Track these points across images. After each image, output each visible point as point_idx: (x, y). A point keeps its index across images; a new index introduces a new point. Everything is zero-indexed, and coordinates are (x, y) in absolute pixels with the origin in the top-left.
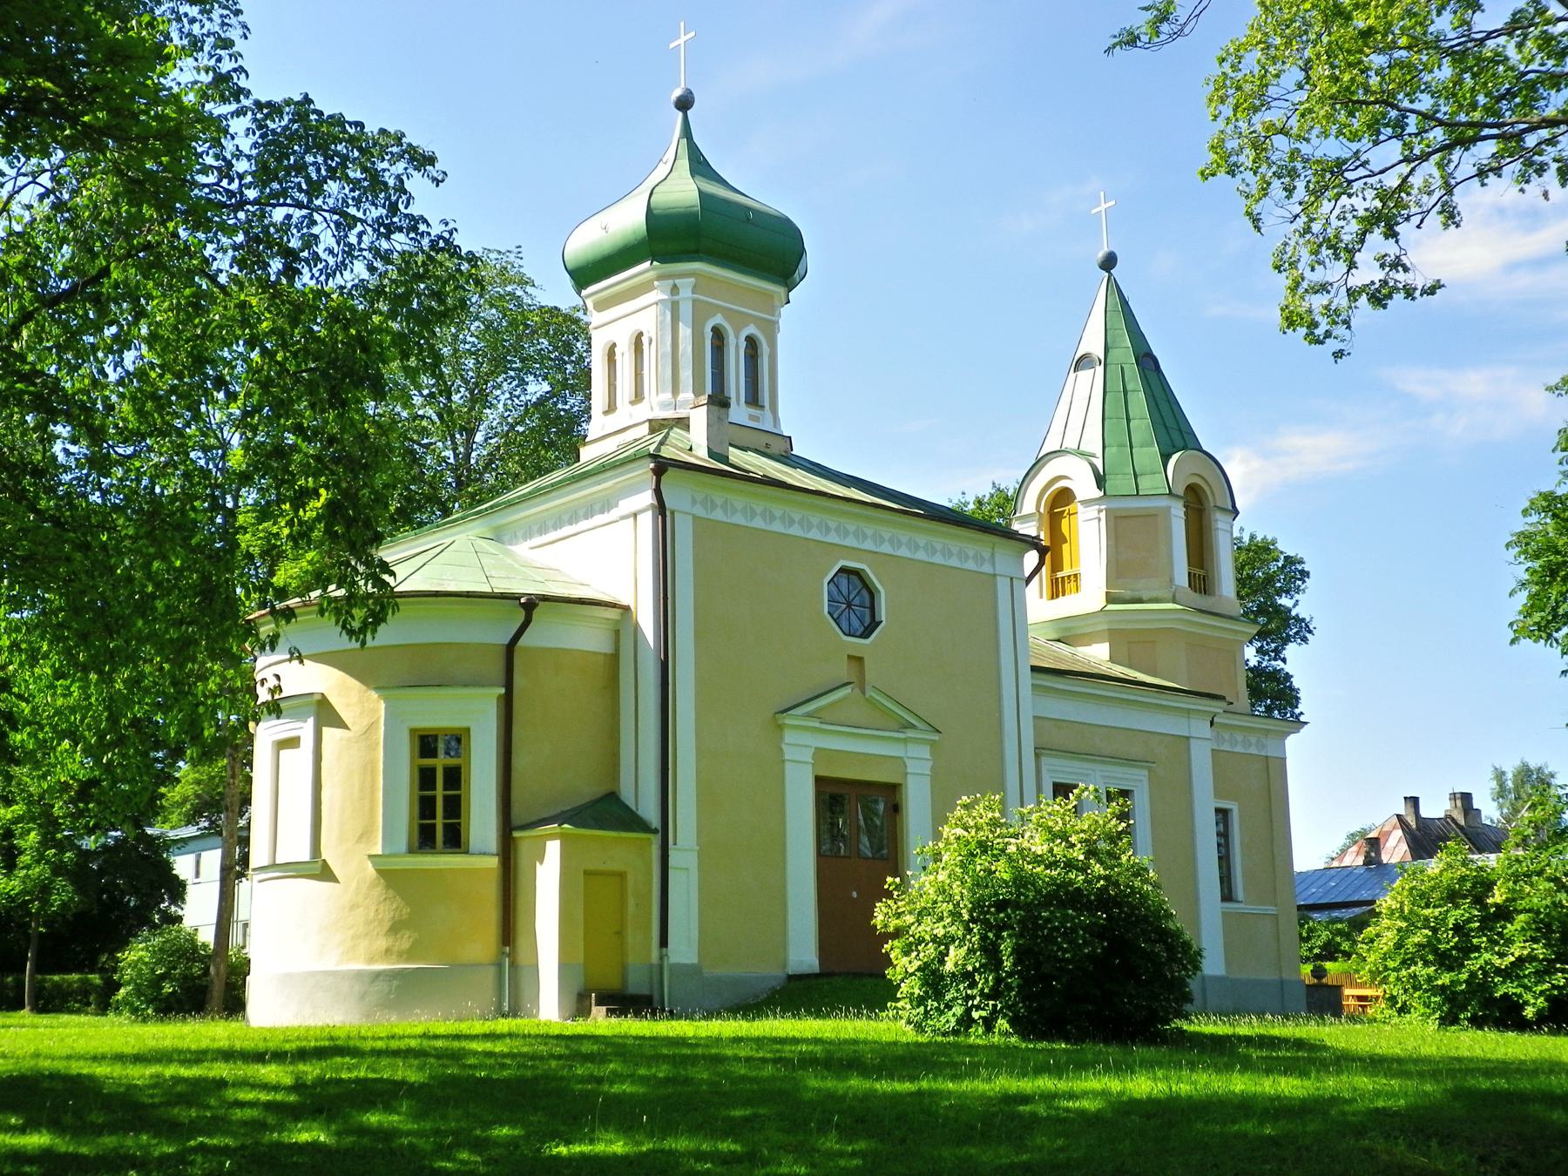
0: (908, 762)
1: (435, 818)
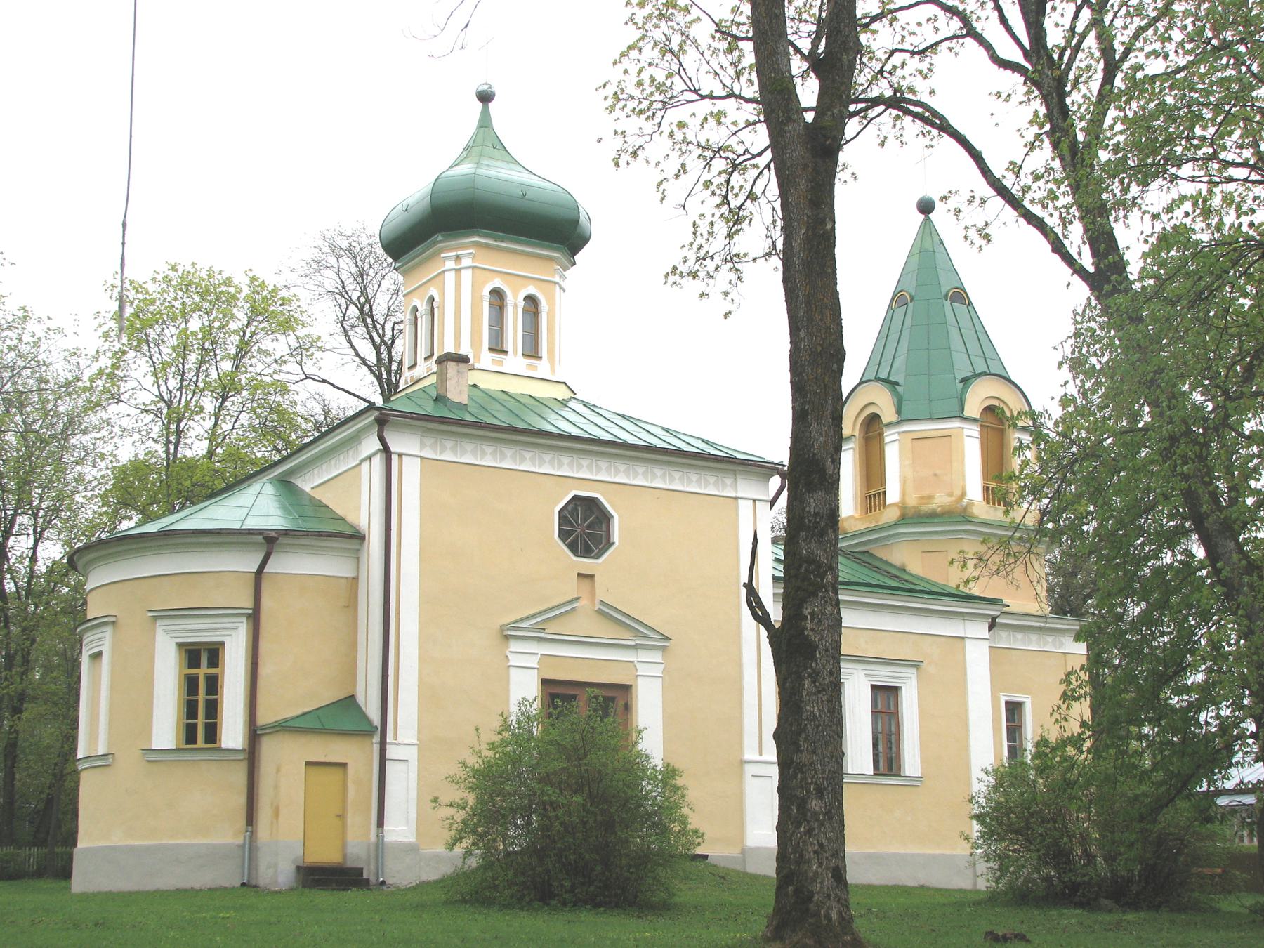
0: (638, 666)
1: (197, 719)
